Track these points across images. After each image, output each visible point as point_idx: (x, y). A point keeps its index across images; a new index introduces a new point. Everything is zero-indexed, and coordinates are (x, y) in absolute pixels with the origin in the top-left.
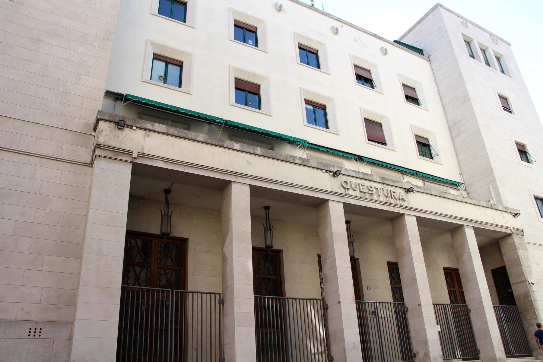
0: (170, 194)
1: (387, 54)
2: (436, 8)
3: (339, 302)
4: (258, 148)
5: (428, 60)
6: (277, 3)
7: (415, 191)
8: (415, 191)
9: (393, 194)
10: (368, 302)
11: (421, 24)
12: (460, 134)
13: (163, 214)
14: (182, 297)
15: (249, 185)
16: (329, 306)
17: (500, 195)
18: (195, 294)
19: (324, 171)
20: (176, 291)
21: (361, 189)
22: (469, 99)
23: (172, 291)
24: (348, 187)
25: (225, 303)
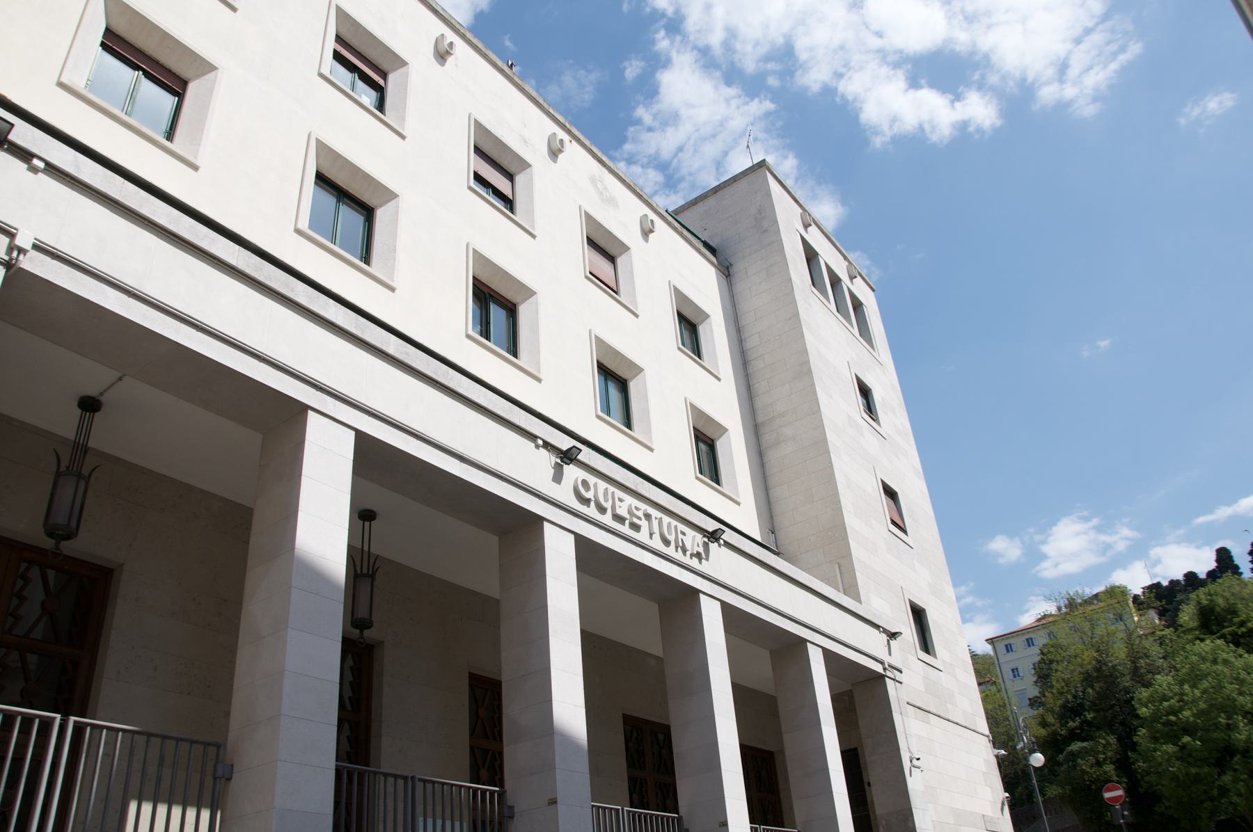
0: (96, 414)
1: (653, 232)
2: (758, 169)
3: (553, 802)
4: (791, 156)
5: (727, 273)
6: (443, 35)
7: (722, 542)
8: (722, 542)
9: (680, 536)
10: (425, 781)
11: (719, 194)
12: (779, 443)
13: (61, 470)
14: (360, 784)
15: (353, 433)
16: (516, 810)
17: (858, 589)
18: (170, 744)
19: (540, 442)
20: (55, 718)
21: (617, 507)
22: (810, 371)
23: (61, 720)
24: (590, 495)
25: (234, 775)
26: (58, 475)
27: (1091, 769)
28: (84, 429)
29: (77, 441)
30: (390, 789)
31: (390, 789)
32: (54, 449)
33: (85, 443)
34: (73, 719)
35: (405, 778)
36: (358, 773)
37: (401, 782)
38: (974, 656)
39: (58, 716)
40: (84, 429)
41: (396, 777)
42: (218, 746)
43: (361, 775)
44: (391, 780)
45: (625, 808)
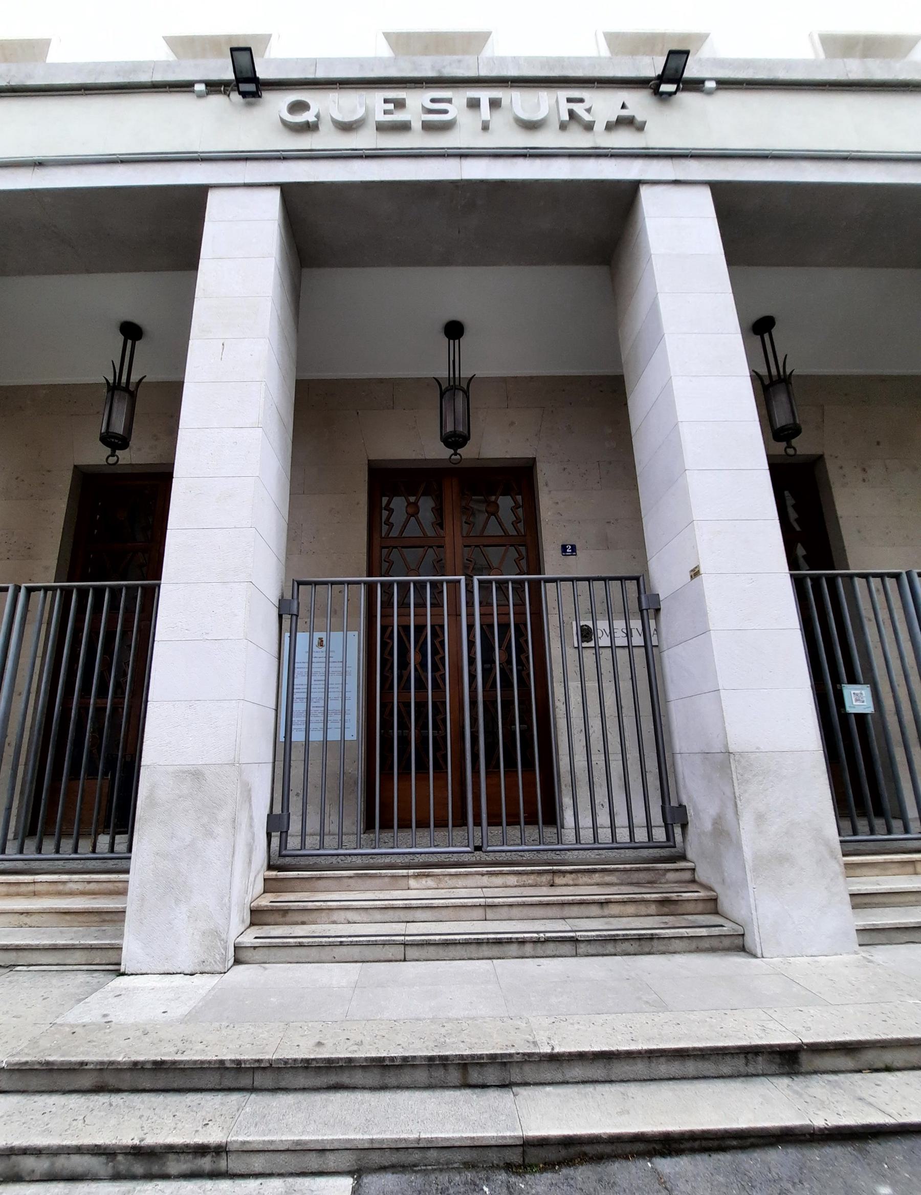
23: (466, 580)
26: (442, 395)
27: (756, 1186)
28: (127, 359)
29: (452, 376)
30: (879, 599)
31: (879, 599)
32: (145, 376)
33: (457, 376)
34: (476, 578)
35: (897, 576)
36: (826, 579)
37: (891, 583)
38: (46, 43)
39: (463, 578)
40: (127, 359)
41: (881, 576)
42: (637, 579)
43: (832, 580)
44: (875, 583)
45: (852, 692)
